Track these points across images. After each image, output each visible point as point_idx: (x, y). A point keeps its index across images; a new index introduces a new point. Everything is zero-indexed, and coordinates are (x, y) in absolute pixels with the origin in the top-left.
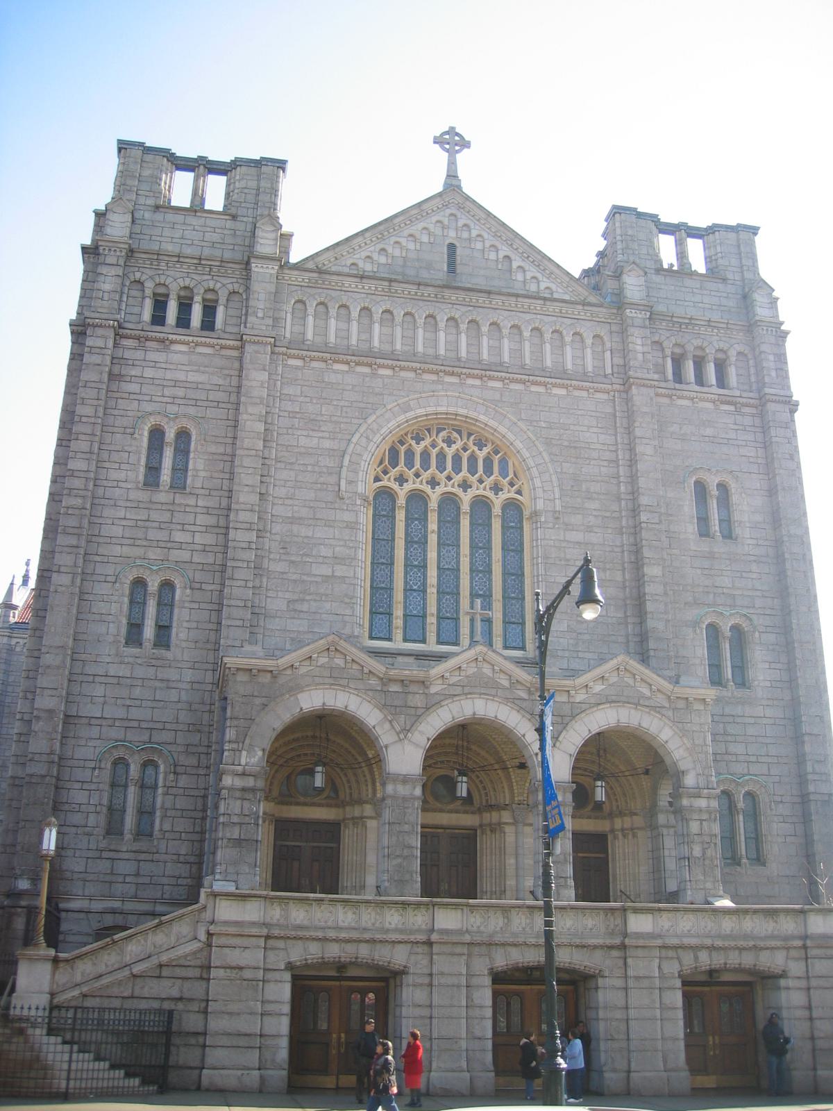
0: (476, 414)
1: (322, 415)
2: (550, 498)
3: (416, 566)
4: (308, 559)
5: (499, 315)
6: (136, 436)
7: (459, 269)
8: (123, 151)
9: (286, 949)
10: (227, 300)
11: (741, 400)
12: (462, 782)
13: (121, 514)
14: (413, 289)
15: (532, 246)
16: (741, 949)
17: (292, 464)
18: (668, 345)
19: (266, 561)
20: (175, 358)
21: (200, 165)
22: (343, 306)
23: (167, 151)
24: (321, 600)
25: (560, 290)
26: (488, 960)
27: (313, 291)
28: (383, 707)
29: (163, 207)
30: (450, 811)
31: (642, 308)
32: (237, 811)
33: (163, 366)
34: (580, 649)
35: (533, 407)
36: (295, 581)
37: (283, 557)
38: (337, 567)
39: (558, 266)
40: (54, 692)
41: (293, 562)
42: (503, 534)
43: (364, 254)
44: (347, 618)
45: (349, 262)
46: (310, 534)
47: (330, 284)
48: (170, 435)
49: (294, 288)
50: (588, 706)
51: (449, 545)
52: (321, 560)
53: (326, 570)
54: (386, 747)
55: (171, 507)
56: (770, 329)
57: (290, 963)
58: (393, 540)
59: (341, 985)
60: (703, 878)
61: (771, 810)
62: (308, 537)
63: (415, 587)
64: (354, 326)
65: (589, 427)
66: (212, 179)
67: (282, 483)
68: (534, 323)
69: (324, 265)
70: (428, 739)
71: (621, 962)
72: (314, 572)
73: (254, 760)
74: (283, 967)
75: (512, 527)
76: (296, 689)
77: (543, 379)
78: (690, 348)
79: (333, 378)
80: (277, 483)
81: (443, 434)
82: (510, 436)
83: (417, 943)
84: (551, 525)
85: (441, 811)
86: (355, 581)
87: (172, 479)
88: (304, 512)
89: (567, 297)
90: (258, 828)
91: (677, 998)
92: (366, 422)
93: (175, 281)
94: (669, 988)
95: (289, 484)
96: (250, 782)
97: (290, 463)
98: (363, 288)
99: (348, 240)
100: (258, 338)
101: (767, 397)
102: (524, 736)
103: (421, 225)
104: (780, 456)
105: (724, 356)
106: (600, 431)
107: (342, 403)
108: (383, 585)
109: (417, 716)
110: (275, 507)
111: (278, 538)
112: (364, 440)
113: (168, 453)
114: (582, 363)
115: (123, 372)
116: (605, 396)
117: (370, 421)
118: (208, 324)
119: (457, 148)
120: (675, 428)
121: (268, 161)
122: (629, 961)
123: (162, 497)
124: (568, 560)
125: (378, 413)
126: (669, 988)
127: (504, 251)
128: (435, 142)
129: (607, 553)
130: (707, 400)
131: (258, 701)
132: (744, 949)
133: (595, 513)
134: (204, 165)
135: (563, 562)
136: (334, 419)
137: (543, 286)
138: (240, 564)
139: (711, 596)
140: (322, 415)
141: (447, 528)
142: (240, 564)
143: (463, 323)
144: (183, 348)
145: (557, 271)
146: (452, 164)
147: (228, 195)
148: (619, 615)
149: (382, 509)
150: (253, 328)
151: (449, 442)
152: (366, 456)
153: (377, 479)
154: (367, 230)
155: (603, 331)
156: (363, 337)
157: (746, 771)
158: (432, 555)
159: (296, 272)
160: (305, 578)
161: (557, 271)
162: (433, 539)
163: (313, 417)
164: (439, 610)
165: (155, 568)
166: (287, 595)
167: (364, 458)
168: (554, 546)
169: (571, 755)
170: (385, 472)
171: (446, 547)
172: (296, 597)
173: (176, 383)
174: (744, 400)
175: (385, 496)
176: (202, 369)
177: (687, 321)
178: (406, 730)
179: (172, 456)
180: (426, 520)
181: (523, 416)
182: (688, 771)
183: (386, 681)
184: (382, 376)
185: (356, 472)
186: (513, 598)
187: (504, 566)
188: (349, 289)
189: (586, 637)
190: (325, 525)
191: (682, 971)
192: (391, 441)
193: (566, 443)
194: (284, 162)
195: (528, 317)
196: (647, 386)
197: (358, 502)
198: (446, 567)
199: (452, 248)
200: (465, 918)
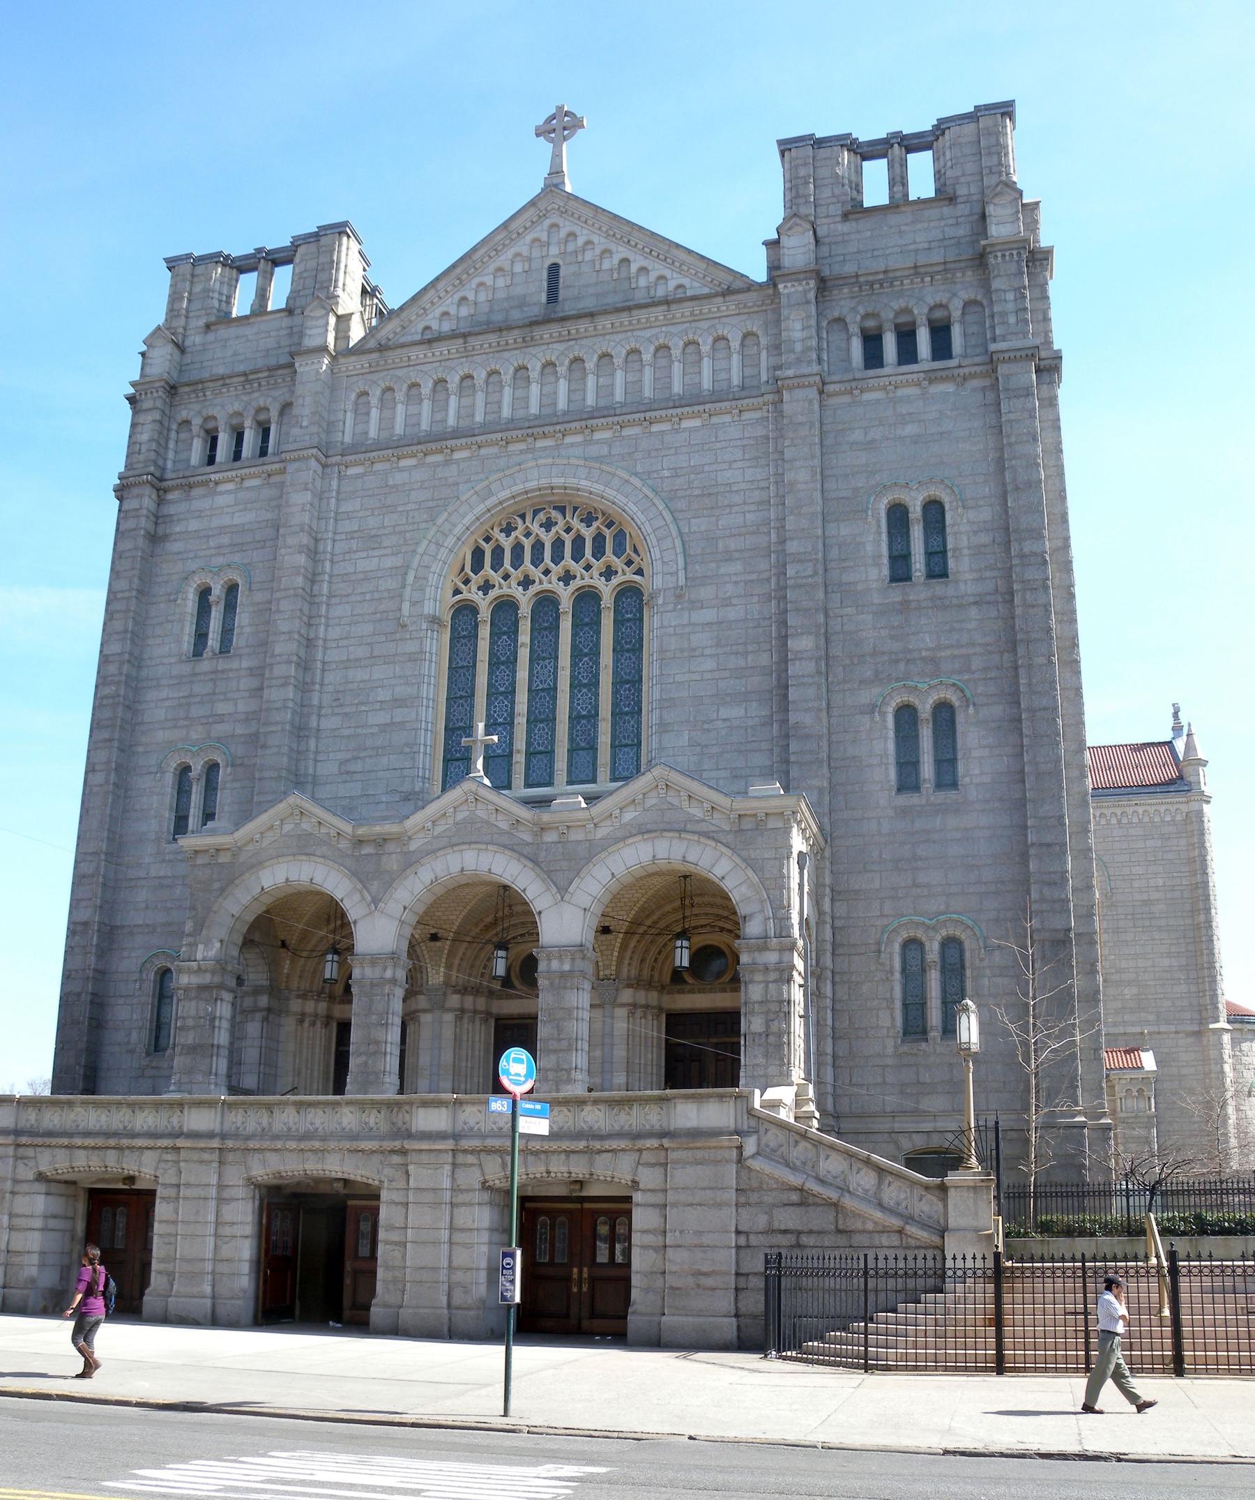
0: (576, 481)
1: (384, 527)
2: (671, 571)
4: (364, 708)
5: (609, 341)
6: (179, 601)
7: (562, 294)
8: (787, 154)
9: (35, 1158)
10: (963, 314)
11: (961, 371)
12: (498, 957)
13: (163, 694)
14: (493, 338)
15: (653, 234)
17: (348, 595)
20: (221, 501)
21: (259, 259)
22: (718, 339)
23: (219, 254)
24: (377, 755)
25: (696, 284)
27: (374, 377)
28: (355, 874)
29: (855, 210)
31: (802, 276)
32: (193, 1012)
33: (209, 513)
34: (706, 767)
37: (336, 710)
38: (398, 711)
39: (690, 252)
41: (346, 714)
42: (616, 630)
43: (438, 312)
44: (406, 772)
45: (420, 327)
46: (367, 677)
47: (394, 362)
48: (916, 512)
49: (355, 379)
51: (544, 659)
52: (378, 706)
53: (383, 718)
54: (355, 922)
55: (213, 676)
56: (1007, 254)
58: (474, 666)
59: (582, 1208)
62: (364, 681)
63: (500, 720)
64: (677, 368)
65: (731, 463)
66: (912, 158)
67: (336, 621)
68: (657, 339)
69: (389, 340)
72: (370, 723)
73: (212, 953)
74: (31, 1177)
75: (629, 620)
76: (257, 865)
77: (663, 413)
79: (398, 478)
81: (542, 517)
82: (620, 499)
83: (166, 1148)
84: (671, 607)
87: (928, 564)
88: (361, 652)
89: (706, 291)
90: (213, 1031)
92: (434, 524)
93: (889, 310)
95: (344, 621)
96: (206, 979)
97: (346, 596)
98: (433, 355)
99: (415, 299)
100: (299, 452)
102: (524, 891)
103: (510, 253)
104: (1013, 439)
105: (946, 313)
106: (747, 464)
109: (390, 882)
110: (328, 652)
112: (433, 547)
113: (917, 533)
114: (728, 376)
115: (168, 531)
116: (757, 415)
117: (440, 521)
118: (942, 348)
119: (566, 132)
120: (857, 435)
121: (326, 230)
122: (411, 1168)
123: (205, 665)
124: (694, 650)
125: (450, 509)
126: (463, 1204)
127: (621, 252)
128: (538, 135)
129: (750, 631)
130: (908, 384)
131: (217, 885)
132: (573, 1152)
133: (734, 579)
134: (899, 143)
135: (686, 654)
138: (274, 728)
139: (902, 666)
140: (384, 527)
141: (543, 637)
142: (274, 728)
143: (562, 365)
144: (230, 486)
145: (689, 259)
146: (557, 156)
147: (939, 175)
148: (763, 714)
149: (462, 629)
150: (295, 441)
151: (548, 525)
152: (436, 567)
153: (457, 592)
154: (437, 279)
155: (755, 326)
157: (942, 908)
158: (522, 675)
159: (353, 358)
160: (359, 731)
161: (689, 259)
162: (524, 654)
163: (373, 532)
164: (529, 744)
165: (195, 749)
166: (340, 756)
167: (432, 570)
168: (675, 634)
169: (585, 909)
170: (467, 582)
171: (541, 662)
172: (349, 756)
173: (222, 530)
174: (966, 370)
175: (465, 611)
176: (249, 506)
177: (881, 276)
178: (376, 901)
179: (922, 537)
180: (516, 632)
181: (639, 469)
182: (751, 915)
183: (359, 842)
184: (457, 462)
185: (423, 590)
187: (615, 673)
188: (418, 362)
189: (715, 750)
190: (385, 663)
192: (472, 541)
193: (697, 492)
194: (1011, 104)
195: (648, 333)
196: (804, 386)
199: (554, 270)
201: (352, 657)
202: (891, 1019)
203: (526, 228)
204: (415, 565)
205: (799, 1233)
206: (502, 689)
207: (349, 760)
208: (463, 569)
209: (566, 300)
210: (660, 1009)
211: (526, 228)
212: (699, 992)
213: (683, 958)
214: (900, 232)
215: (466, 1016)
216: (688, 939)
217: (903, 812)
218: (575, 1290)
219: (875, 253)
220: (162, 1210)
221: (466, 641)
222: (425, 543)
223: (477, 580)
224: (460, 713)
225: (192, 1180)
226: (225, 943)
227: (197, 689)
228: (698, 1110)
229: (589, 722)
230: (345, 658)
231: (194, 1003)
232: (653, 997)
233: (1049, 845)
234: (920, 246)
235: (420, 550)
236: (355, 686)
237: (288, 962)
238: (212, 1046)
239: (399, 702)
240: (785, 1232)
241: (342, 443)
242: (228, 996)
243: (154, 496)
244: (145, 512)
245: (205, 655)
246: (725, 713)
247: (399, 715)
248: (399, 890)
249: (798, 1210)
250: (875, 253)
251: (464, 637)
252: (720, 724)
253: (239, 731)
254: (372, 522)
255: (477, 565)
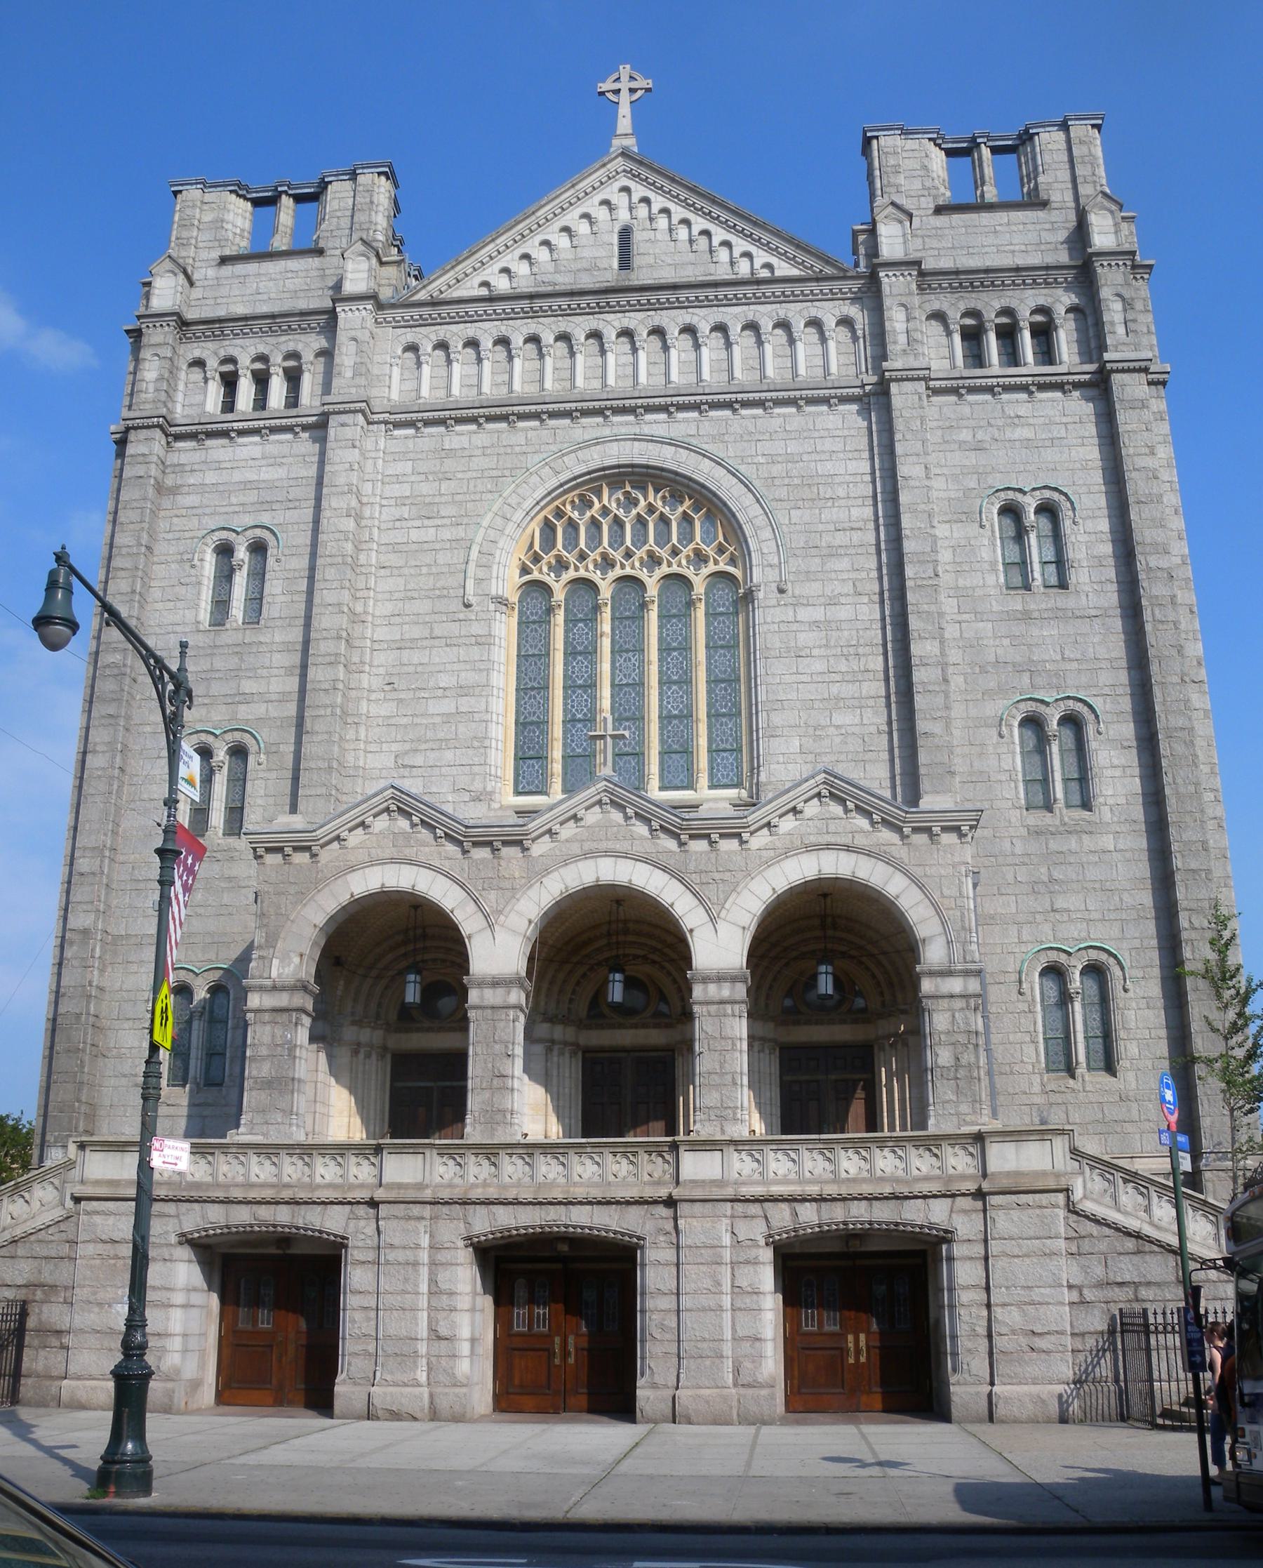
3: (581, 686)
9: (177, 1216)
12: (614, 981)
16: (871, 1199)
18: (954, 315)
19: (364, 703)
26: (462, 1225)
30: (635, 1026)
35: (746, 437)
36: (405, 726)
40: (89, 907)
41: (400, 701)
44: (476, 769)
46: (426, 660)
50: (772, 853)
51: (627, 651)
53: (447, 706)
57: (183, 1235)
60: (954, 1098)
61: (1126, 991)
63: (579, 716)
69: (441, 292)
70: (530, 922)
71: (669, 1226)
75: (721, 614)
78: (990, 315)
80: (380, 596)
84: (774, 602)
85: (621, 1026)
86: (488, 717)
88: (416, 632)
91: (766, 1277)
94: (748, 1262)
101: (1109, 366)
107: (469, 475)
108: (535, 719)
111: (382, 671)
123: (227, 637)
124: (801, 650)
136: (458, 498)
137: (758, 263)
153: (525, 570)
155: (853, 311)
156: (500, 379)
157: (1084, 934)
170: (537, 559)
171: (625, 655)
172: (407, 746)
173: (246, 485)
186: (724, 715)
191: (770, 1236)
197: (492, 607)
198: (624, 682)
200: (427, 1167)
201: (407, 636)
202: (1033, 1054)
203: (594, 189)
204: (479, 539)
205: (1136, 1285)
206: (580, 682)
207: (406, 753)
208: (531, 545)
209: (639, 267)
210: (578, 1045)
211: (602, 183)
212: (816, 1024)
213: (412, 994)
214: (996, 232)
215: (556, 1047)
216: (831, 964)
217: (1036, 833)
218: (851, 1361)
219: (971, 250)
220: (356, 1277)
221: (536, 626)
222: (490, 515)
223: (549, 558)
224: (531, 706)
225: (396, 1242)
226: (305, 958)
227: (219, 663)
228: (1017, 1151)
229: (681, 722)
230: (398, 637)
231: (268, 1028)
232: (569, 1033)
233: (1193, 871)
234: (1017, 248)
235: (485, 523)
236: (411, 669)
237: (342, 983)
238: (293, 1079)
239: (463, 691)
240: (1121, 1284)
241: (389, 400)
242: (307, 1021)
243: (164, 442)
244: (155, 459)
245: (228, 626)
246: (838, 719)
247: (465, 704)
248: (522, 901)
249: (1136, 1259)
250: (971, 250)
251: (534, 622)
252: (832, 730)
253: (274, 713)
254: (425, 488)
255: (548, 542)
